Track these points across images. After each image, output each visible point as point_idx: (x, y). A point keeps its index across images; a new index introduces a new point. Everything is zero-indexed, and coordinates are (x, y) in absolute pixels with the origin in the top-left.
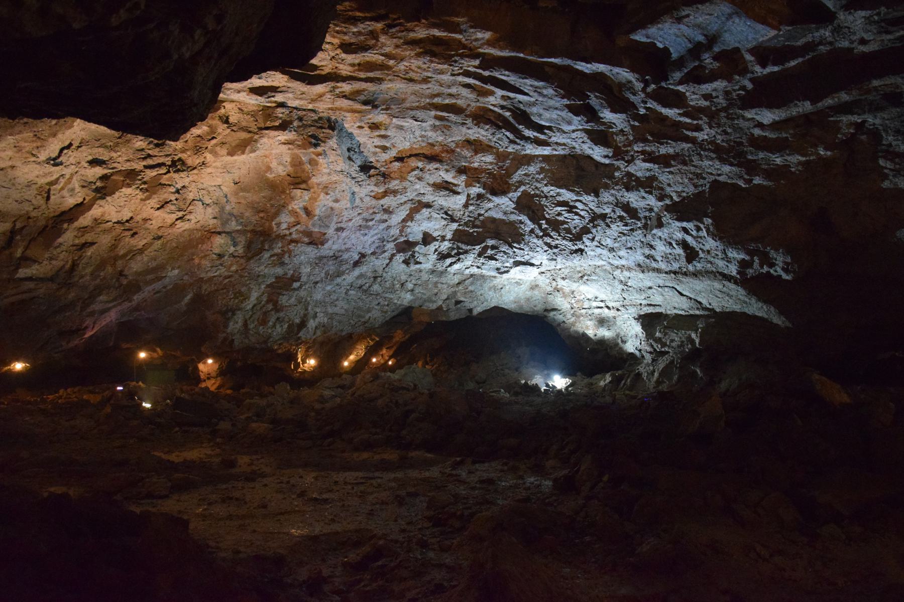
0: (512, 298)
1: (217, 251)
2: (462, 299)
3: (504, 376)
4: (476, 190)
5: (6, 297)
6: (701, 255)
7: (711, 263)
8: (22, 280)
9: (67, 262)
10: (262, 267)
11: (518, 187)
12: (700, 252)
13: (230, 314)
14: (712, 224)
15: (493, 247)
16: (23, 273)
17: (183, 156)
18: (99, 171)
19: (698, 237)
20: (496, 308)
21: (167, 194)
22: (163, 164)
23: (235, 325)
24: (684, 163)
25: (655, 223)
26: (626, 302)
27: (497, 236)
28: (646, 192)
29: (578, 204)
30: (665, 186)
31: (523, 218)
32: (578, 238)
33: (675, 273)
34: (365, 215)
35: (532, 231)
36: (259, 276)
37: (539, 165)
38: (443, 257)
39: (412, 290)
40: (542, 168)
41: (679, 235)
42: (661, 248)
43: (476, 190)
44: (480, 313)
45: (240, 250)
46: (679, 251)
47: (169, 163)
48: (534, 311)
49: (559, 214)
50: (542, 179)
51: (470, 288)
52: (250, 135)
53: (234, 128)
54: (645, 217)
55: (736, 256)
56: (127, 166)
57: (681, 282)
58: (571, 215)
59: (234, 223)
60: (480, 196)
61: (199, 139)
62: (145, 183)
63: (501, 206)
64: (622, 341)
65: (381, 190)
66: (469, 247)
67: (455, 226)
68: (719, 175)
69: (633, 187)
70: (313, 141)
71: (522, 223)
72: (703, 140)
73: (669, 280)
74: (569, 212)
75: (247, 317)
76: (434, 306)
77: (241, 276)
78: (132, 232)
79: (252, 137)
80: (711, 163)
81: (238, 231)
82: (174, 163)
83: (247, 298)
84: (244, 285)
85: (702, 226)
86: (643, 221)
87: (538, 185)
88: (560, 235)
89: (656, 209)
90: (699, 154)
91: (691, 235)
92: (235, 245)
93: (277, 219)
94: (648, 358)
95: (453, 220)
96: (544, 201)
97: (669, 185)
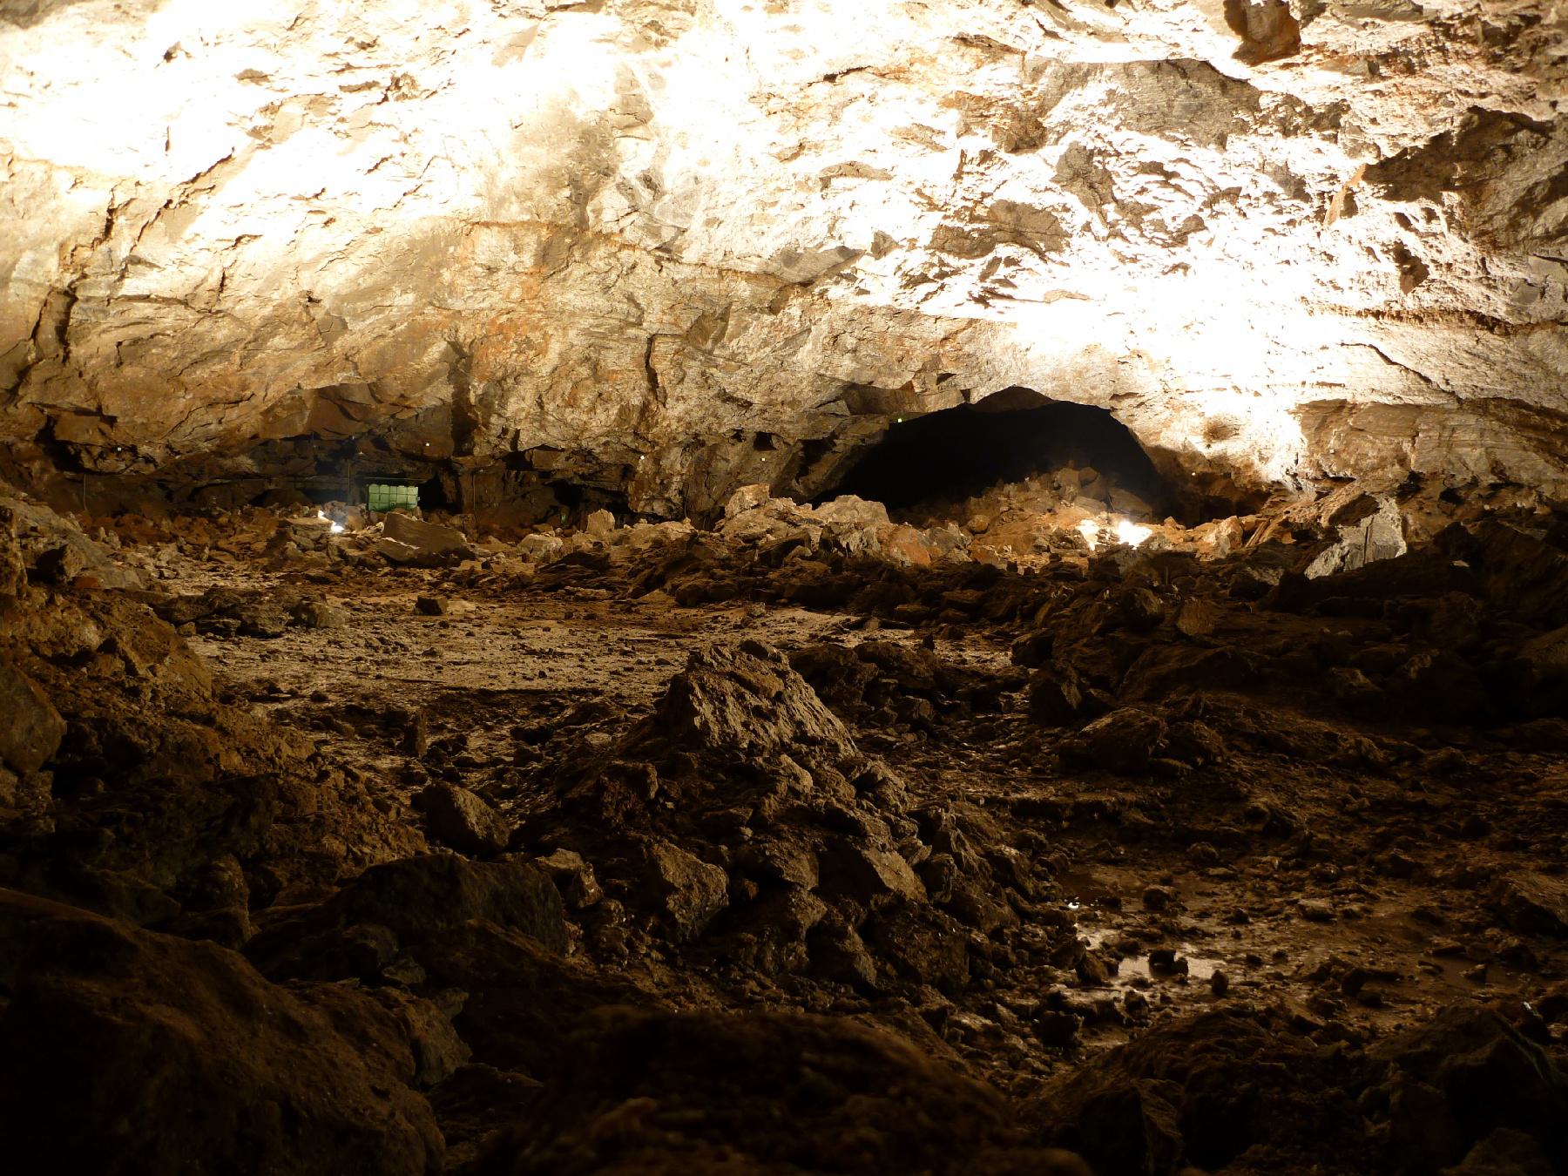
0: (1048, 371)
1: (483, 258)
2: (950, 370)
3: (1023, 520)
4: (981, 140)
5: (104, 331)
6: (1434, 273)
7: (1453, 291)
8: (130, 299)
9: (212, 270)
10: (570, 296)
11: (1060, 135)
12: (1432, 268)
13: (510, 381)
14: (1461, 204)
15: (1010, 262)
16: (131, 286)
17: (411, 69)
18: (260, 95)
19: (1428, 234)
20: (1016, 395)
21: (379, 143)
22: (374, 84)
23: (519, 405)
24: (1410, 70)
25: (1339, 204)
26: (1273, 380)
27: (1018, 238)
28: (1325, 138)
29: (1181, 168)
30: (1366, 124)
31: (1072, 199)
32: (1180, 239)
33: (1378, 314)
34: (762, 194)
35: (1087, 227)
36: (562, 312)
37: (1106, 86)
38: (913, 282)
39: (855, 351)
40: (1111, 93)
41: (1395, 232)
42: (1351, 262)
43: (981, 140)
44: (985, 401)
45: (528, 260)
46: (1390, 267)
47: (388, 83)
48: (1091, 398)
49: (1143, 191)
50: (1110, 116)
51: (967, 349)
52: (533, 22)
53: (504, 11)
54: (1321, 194)
55: (1507, 272)
56: (314, 87)
57: (1388, 333)
58: (1168, 193)
59: (515, 208)
60: (986, 156)
61: (439, 33)
62: (342, 120)
63: (1028, 179)
64: (1261, 458)
65: (792, 141)
66: (964, 262)
67: (935, 218)
68: (1483, 96)
69: (1297, 128)
70: (654, 36)
71: (1068, 210)
72: (1451, 18)
73: (1365, 330)
74: (1166, 184)
75: (543, 390)
76: (895, 384)
77: (530, 311)
78: (325, 218)
79: (535, 28)
80: (1465, 68)
81: (523, 223)
82: (396, 83)
83: (542, 351)
84: (535, 328)
85: (1438, 210)
86: (1316, 203)
87: (1102, 129)
88: (1142, 235)
89: (1343, 178)
90: (1442, 49)
91: (1416, 231)
92: (518, 249)
93: (595, 201)
94: (1310, 489)
95: (932, 206)
96: (1112, 164)
97: (1374, 121)
